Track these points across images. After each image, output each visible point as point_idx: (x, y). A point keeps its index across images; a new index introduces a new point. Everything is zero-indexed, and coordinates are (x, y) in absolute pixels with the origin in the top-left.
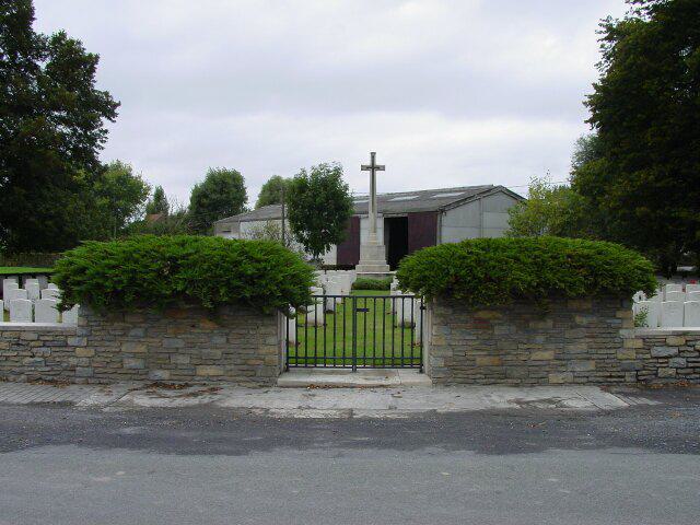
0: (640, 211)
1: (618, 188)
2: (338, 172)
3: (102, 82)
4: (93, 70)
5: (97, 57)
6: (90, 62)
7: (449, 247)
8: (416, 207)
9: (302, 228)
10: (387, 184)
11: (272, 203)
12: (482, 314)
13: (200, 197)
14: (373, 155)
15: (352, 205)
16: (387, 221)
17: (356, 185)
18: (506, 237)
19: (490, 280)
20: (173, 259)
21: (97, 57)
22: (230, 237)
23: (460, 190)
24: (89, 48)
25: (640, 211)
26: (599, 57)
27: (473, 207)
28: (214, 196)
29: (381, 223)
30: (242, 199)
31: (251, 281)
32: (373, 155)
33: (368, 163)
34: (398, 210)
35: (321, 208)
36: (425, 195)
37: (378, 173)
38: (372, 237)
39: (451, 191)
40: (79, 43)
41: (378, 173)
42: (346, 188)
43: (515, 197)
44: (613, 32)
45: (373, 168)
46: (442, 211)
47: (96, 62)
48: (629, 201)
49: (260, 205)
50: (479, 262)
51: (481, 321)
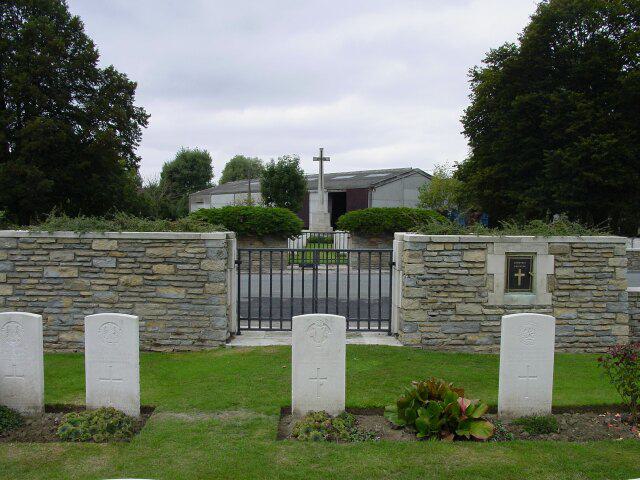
0: (487, 192)
1: (476, 178)
2: (296, 162)
3: (138, 101)
4: (132, 93)
5: (136, 84)
6: (130, 88)
7: (377, 211)
8: (353, 185)
9: (271, 200)
10: (329, 169)
11: (234, 179)
12: (372, 240)
13: (171, 173)
14: (321, 150)
15: (306, 183)
16: (330, 195)
17: (308, 168)
18: (416, 208)
19: (375, 224)
20: (244, 215)
21: (136, 84)
22: (206, 206)
23: (387, 171)
24: (131, 79)
25: (487, 192)
26: (470, 92)
27: (395, 186)
28: (186, 172)
29: (326, 197)
30: (209, 176)
31: (278, 224)
32: (321, 150)
33: (318, 156)
34: (339, 187)
35: (284, 187)
36: (360, 175)
37: (325, 163)
38: (318, 207)
39: (379, 172)
40: (125, 75)
41: (325, 163)
42: (302, 172)
43: (428, 176)
44: (477, 77)
45: (322, 159)
46: (372, 188)
47: (135, 88)
48: (482, 185)
49: (224, 181)
50: (371, 218)
51: (372, 242)
